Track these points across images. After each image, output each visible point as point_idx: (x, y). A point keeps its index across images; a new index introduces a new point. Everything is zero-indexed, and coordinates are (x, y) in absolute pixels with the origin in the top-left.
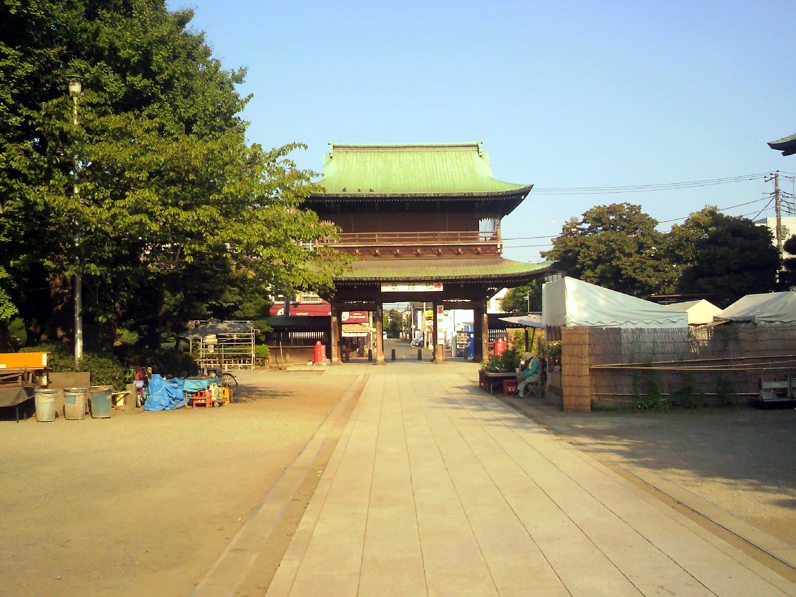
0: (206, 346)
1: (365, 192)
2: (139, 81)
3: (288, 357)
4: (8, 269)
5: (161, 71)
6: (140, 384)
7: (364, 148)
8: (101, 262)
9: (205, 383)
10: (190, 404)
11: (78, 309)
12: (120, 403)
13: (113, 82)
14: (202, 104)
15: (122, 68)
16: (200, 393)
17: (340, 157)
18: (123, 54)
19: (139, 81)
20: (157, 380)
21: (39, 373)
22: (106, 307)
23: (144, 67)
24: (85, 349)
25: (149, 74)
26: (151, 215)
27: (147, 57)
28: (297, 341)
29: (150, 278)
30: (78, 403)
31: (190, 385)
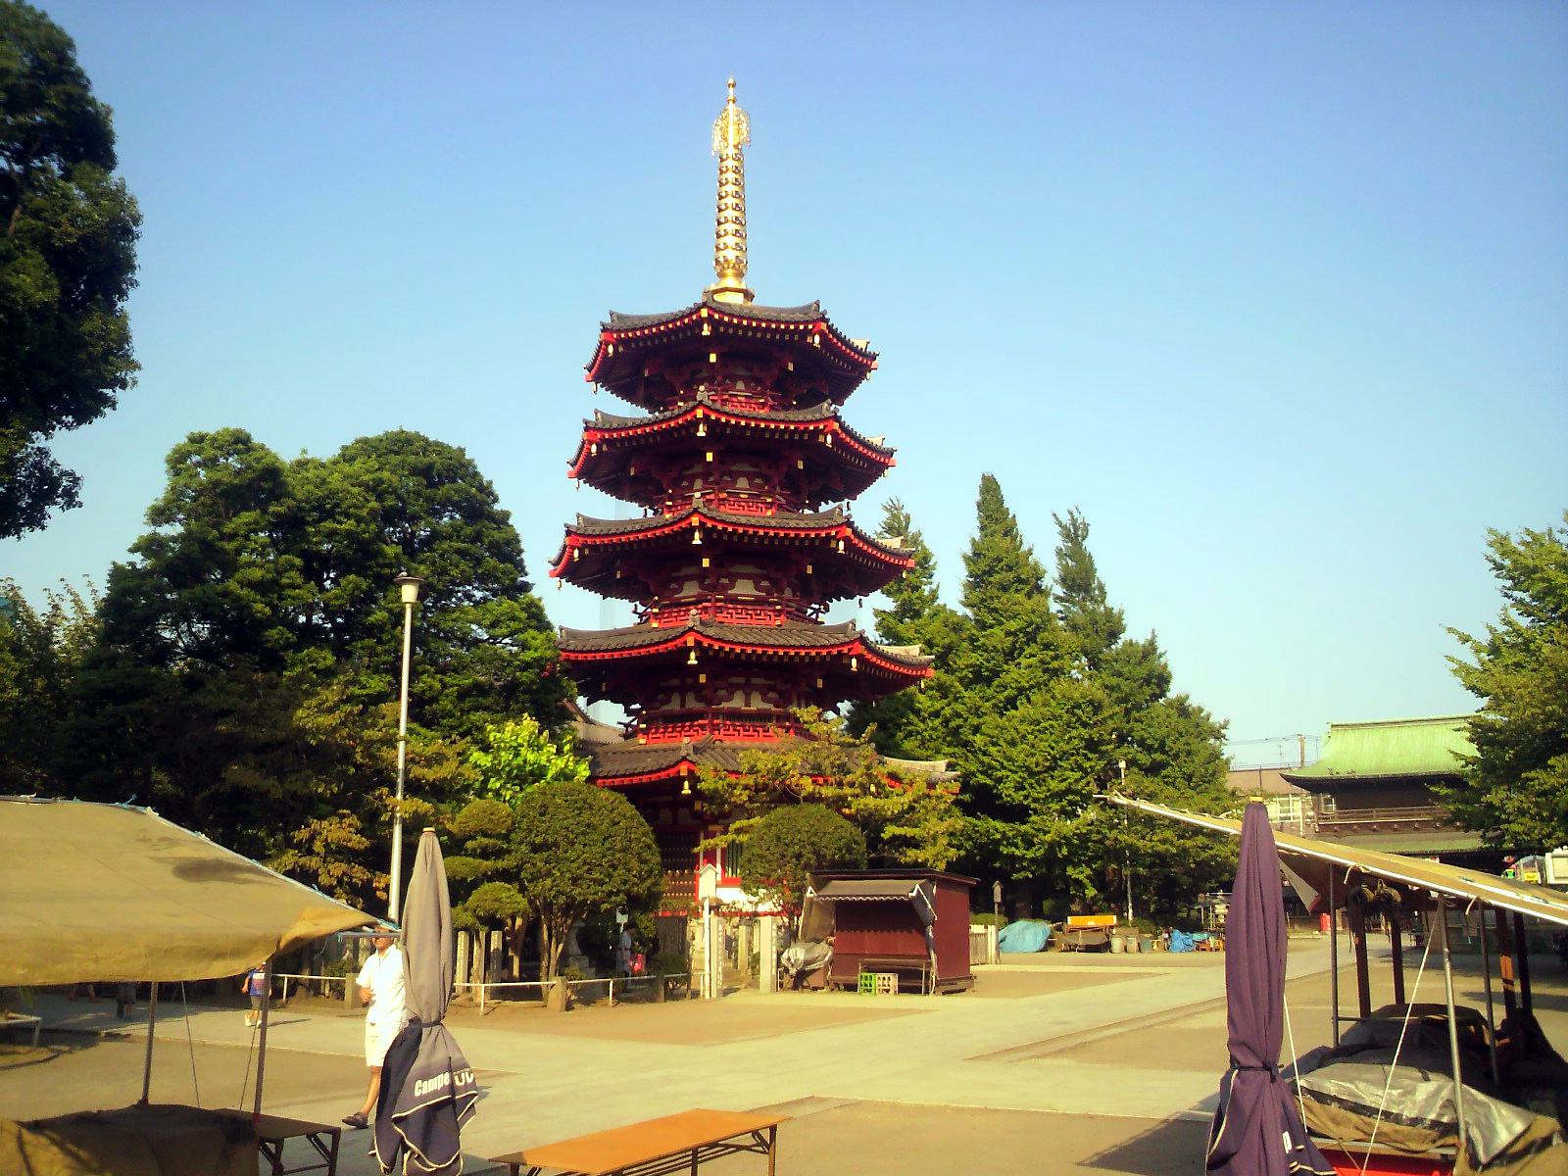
0: (1217, 916)
1: (1343, 774)
2: (1158, 757)
3: (1296, 927)
4: (1092, 869)
5: (1172, 749)
6: (1167, 936)
7: (1363, 725)
8: (1143, 866)
9: (1206, 935)
10: (1197, 949)
11: (1129, 891)
12: (1155, 947)
13: (1144, 759)
14: (1195, 766)
15: (1149, 749)
16: (1203, 942)
17: (1339, 735)
18: (1149, 742)
19: (1158, 757)
20: (1177, 933)
21: (1112, 927)
22: (1146, 890)
23: (1162, 749)
24: (1134, 915)
25: (1164, 752)
26: (1172, 844)
27: (1162, 744)
28: (735, 715)
29: (997, 865)
30: (1133, 943)
31: (1197, 937)
